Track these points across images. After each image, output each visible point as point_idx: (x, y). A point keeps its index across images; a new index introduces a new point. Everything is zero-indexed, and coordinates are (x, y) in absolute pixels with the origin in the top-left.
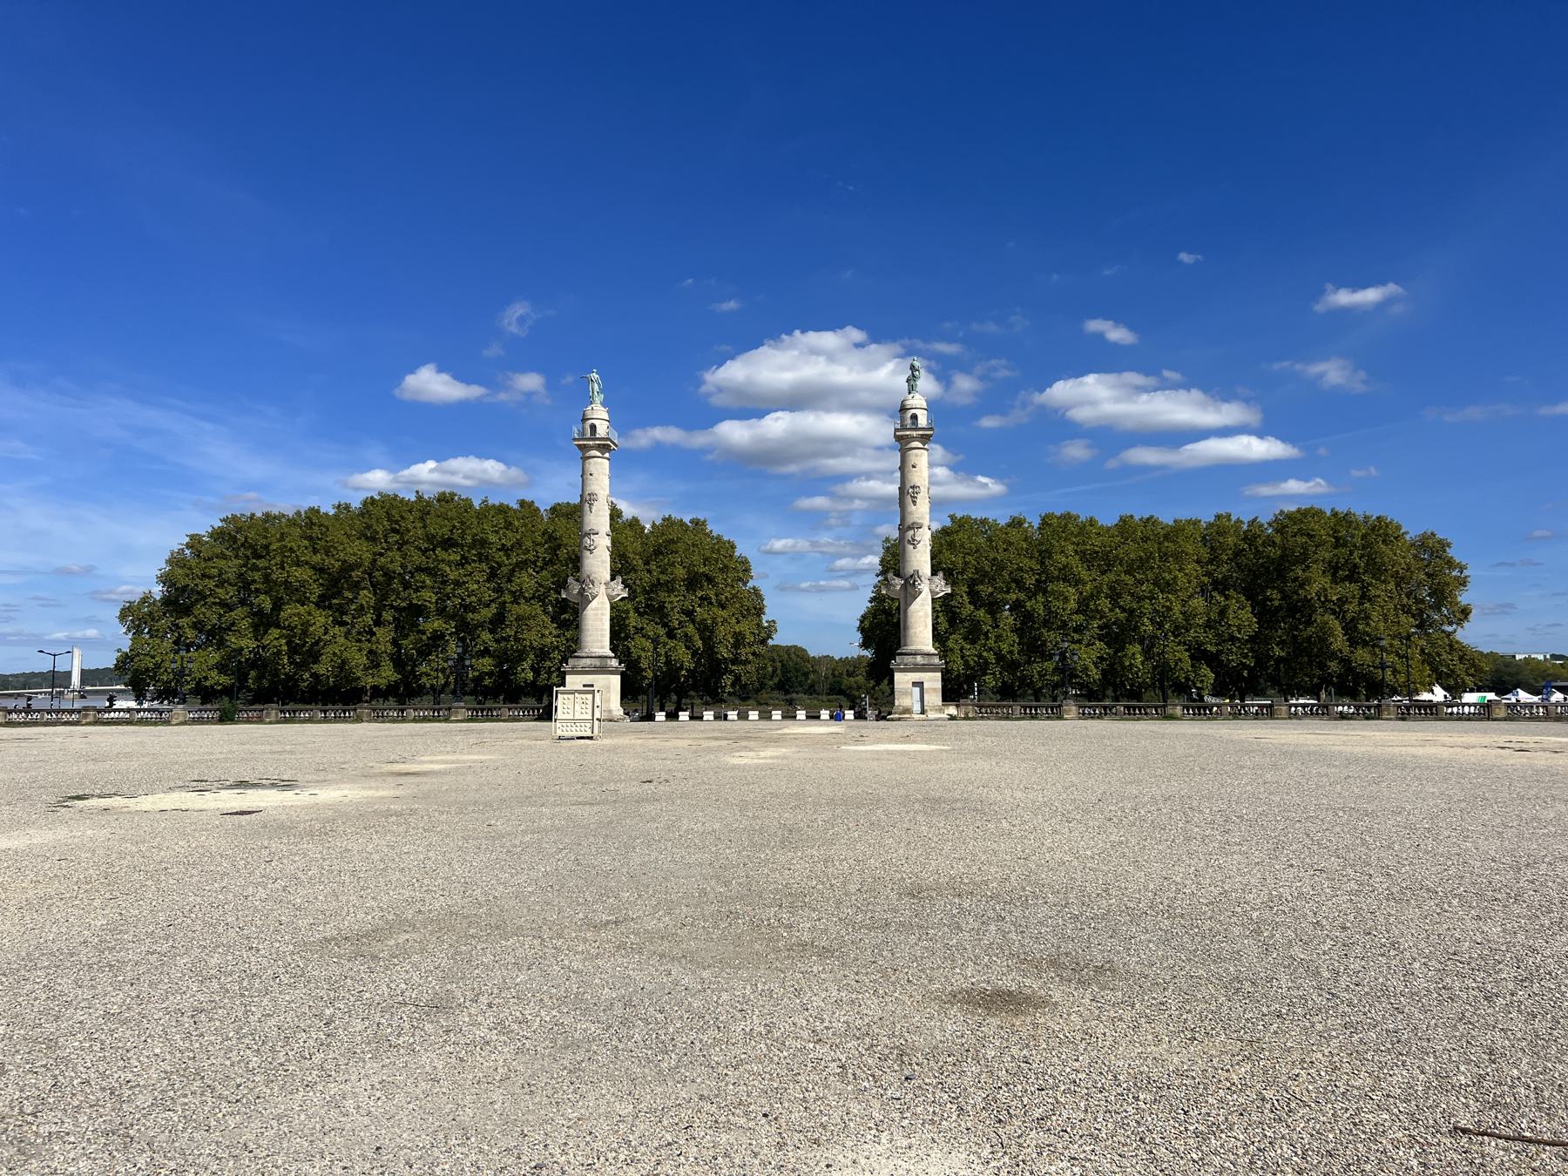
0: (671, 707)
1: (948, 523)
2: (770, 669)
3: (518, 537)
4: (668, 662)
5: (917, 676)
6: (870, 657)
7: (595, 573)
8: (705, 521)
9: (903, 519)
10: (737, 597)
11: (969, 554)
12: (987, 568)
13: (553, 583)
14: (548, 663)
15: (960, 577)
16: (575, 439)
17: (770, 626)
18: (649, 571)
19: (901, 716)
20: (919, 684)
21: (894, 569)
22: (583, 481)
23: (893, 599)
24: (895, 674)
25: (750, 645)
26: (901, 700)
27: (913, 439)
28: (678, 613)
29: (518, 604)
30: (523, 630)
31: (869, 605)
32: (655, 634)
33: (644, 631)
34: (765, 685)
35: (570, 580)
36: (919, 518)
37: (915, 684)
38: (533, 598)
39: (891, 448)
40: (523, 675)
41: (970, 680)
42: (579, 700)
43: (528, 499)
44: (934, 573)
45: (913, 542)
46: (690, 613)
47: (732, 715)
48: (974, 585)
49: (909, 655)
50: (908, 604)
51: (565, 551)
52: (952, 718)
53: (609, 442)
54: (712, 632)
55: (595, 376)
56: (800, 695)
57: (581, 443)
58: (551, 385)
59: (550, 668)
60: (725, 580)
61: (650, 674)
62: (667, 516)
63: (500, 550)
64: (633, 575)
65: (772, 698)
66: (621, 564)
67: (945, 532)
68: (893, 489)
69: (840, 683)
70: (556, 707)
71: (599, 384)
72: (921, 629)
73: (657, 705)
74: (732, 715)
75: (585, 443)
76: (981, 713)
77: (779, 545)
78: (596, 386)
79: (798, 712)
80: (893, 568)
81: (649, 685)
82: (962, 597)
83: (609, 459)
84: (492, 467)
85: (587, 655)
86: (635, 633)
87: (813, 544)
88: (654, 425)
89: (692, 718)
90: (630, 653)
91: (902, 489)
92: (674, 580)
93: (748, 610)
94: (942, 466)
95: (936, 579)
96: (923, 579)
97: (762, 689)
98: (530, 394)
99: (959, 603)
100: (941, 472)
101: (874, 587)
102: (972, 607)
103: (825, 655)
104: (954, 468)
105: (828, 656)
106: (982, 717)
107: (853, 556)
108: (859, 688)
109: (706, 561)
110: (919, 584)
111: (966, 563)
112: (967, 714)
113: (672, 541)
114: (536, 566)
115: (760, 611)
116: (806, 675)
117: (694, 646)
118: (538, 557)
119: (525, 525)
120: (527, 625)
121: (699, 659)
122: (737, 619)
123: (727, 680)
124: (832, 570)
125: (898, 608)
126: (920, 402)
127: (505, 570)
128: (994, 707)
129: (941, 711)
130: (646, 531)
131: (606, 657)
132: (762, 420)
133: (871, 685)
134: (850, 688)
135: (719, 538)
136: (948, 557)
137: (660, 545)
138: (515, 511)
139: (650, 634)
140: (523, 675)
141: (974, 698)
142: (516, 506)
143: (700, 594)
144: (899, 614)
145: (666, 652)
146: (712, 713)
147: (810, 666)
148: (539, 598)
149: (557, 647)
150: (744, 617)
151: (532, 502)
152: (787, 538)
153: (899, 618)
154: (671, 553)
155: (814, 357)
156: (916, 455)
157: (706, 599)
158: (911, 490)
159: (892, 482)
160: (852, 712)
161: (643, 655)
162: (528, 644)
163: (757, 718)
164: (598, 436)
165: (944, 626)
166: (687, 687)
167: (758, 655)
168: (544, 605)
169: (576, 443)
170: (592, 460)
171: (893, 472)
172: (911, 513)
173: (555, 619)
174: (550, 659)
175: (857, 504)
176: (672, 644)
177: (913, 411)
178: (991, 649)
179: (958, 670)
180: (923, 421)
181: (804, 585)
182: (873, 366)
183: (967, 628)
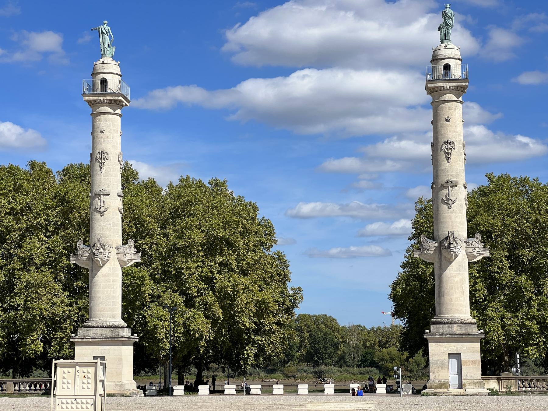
0: (191, 379)
1: (486, 183)
2: (297, 340)
3: (28, 201)
4: (187, 332)
5: (454, 347)
6: (403, 326)
7: (106, 237)
8: (225, 182)
9: (436, 176)
10: (260, 263)
11: (508, 216)
12: (528, 231)
13: (64, 249)
14: (60, 334)
15: (499, 240)
16: (84, 95)
17: (295, 294)
18: (166, 236)
19: (437, 391)
20: (457, 356)
21: (429, 232)
22: (93, 138)
23: (427, 264)
24: (430, 344)
25: (275, 314)
26: (436, 373)
27: (447, 91)
28: (196, 280)
29: (28, 271)
30: (32, 298)
31: (402, 271)
32: (172, 302)
33: (161, 299)
34: (292, 356)
35: (80, 244)
36: (454, 176)
37: (451, 356)
38: (43, 264)
39: (424, 107)
40: (33, 346)
41: (511, 351)
42: (80, 374)
43: (39, 160)
44: (471, 235)
45: (448, 202)
46: (209, 281)
47: (255, 388)
48: (514, 249)
49: (445, 324)
50: (442, 269)
51: (77, 214)
52: (493, 393)
53: (120, 98)
54: (233, 300)
55: (106, 28)
56: (330, 367)
57: (91, 98)
58: (68, 45)
59: (62, 338)
60: (247, 244)
61: (166, 345)
62: (185, 177)
63: (9, 214)
64: (148, 240)
65: (299, 371)
66: (136, 228)
67: (482, 192)
68: (427, 149)
69: (371, 354)
70: (55, 381)
71: (110, 36)
72: (457, 295)
73: (174, 377)
74: (255, 388)
75: (96, 98)
76: (524, 386)
77: (306, 208)
78: (107, 38)
79: (326, 386)
80: (426, 231)
81: (166, 356)
82: (501, 261)
83: (120, 115)
84: (9, 130)
85: (97, 325)
86: (152, 302)
87: (343, 208)
88: (175, 84)
89: (212, 392)
90: (146, 322)
91: (435, 145)
92: (192, 245)
93: (272, 276)
94: (479, 124)
95: (472, 240)
96: (458, 241)
97: (289, 360)
98: (46, 54)
99: (498, 268)
100: (478, 131)
101: (407, 252)
102: (513, 273)
103: (355, 325)
104: (492, 127)
105: (359, 326)
106: (525, 392)
107: (385, 220)
108: (392, 359)
109: (226, 224)
110: (455, 247)
111: (505, 225)
112: (509, 388)
113: (189, 204)
114: (47, 230)
115: (284, 278)
116: (336, 345)
117: (214, 315)
118: (50, 222)
119: (35, 188)
120: (37, 293)
121: (220, 329)
122: (260, 286)
123: (250, 351)
124: (363, 235)
125: (432, 274)
126: (453, 51)
127: (14, 235)
128: (538, 380)
129: (481, 385)
130: (162, 193)
131: (119, 327)
132: (288, 78)
133: (405, 357)
134: (383, 359)
135: (239, 201)
136: (484, 218)
137: (178, 208)
138: (25, 173)
139: (168, 302)
140: (33, 346)
141: (517, 371)
142: (27, 168)
143: (219, 259)
144: (434, 279)
145: (184, 323)
146: (234, 386)
147: (339, 336)
148: (51, 265)
149: (69, 317)
150: (267, 285)
151: (44, 163)
152: (316, 201)
153: (434, 285)
154: (189, 216)
155: (342, 13)
156: (450, 109)
157: (226, 265)
158: (444, 146)
159: (425, 143)
160: (384, 386)
161: (160, 324)
162: (38, 313)
163: (281, 392)
164: (109, 91)
165: (482, 292)
166: (208, 357)
167: (283, 325)
168: (56, 272)
169: (87, 98)
170: (103, 117)
171: (426, 132)
172: (445, 171)
173: (67, 287)
174: (62, 329)
175: (389, 165)
176: (190, 312)
177: (446, 61)
178: (534, 318)
179: (499, 341)
180: (456, 71)
181: (334, 251)
182: (405, 22)
183: (507, 295)
